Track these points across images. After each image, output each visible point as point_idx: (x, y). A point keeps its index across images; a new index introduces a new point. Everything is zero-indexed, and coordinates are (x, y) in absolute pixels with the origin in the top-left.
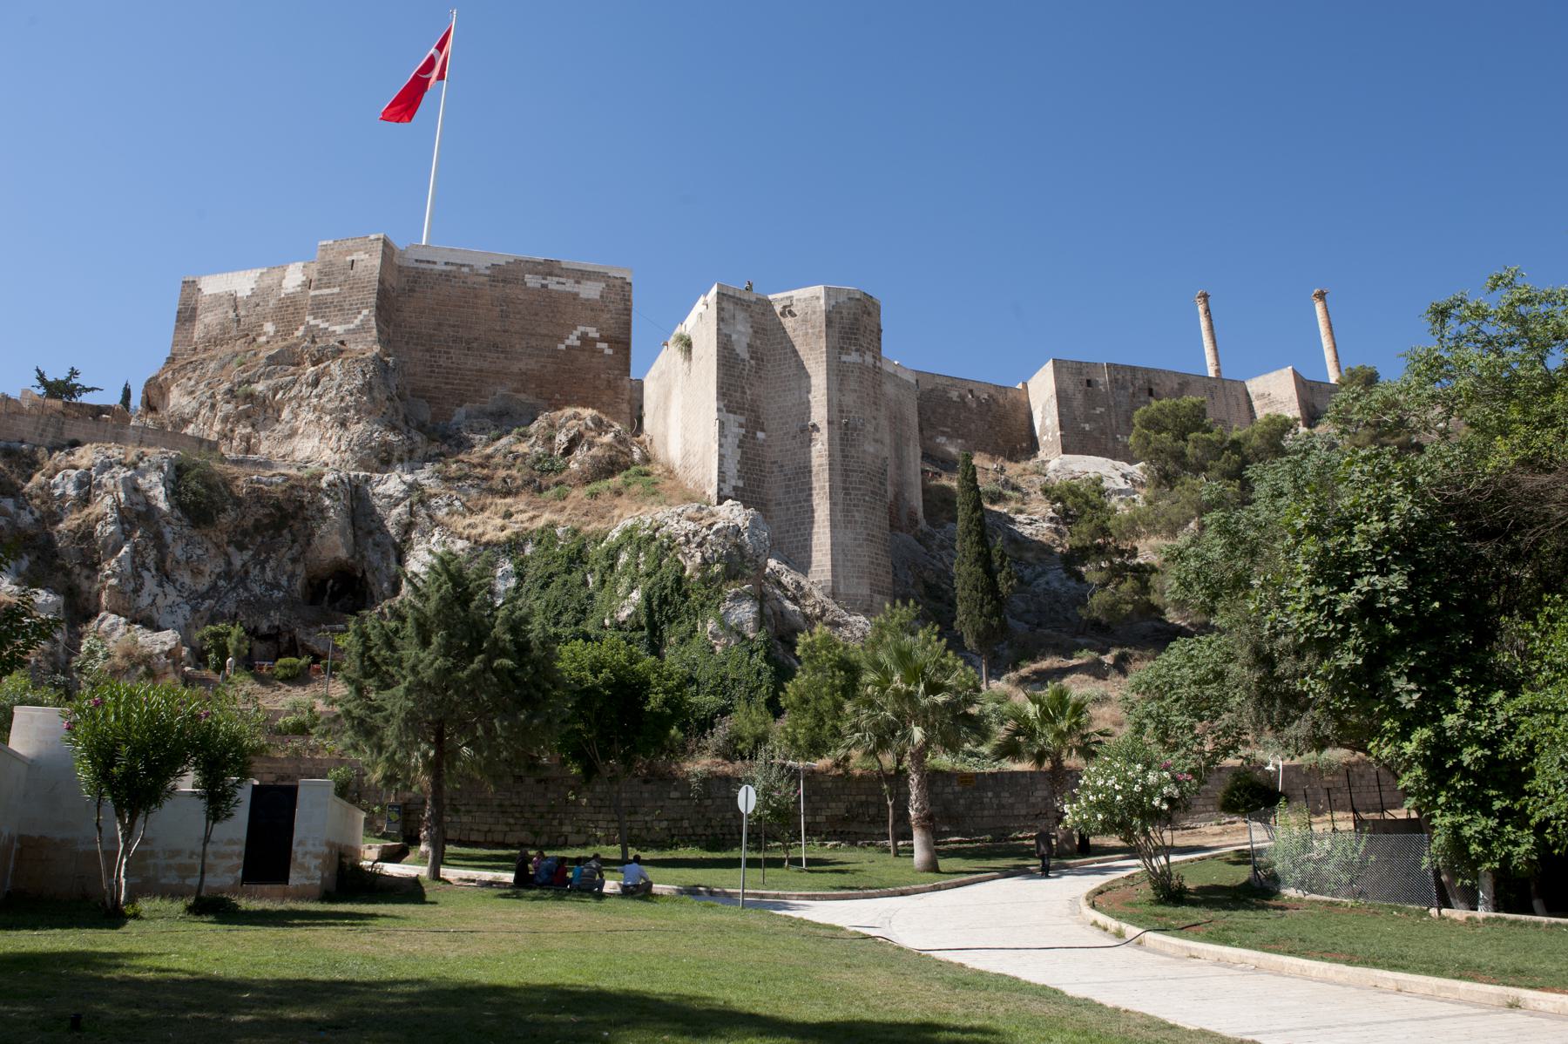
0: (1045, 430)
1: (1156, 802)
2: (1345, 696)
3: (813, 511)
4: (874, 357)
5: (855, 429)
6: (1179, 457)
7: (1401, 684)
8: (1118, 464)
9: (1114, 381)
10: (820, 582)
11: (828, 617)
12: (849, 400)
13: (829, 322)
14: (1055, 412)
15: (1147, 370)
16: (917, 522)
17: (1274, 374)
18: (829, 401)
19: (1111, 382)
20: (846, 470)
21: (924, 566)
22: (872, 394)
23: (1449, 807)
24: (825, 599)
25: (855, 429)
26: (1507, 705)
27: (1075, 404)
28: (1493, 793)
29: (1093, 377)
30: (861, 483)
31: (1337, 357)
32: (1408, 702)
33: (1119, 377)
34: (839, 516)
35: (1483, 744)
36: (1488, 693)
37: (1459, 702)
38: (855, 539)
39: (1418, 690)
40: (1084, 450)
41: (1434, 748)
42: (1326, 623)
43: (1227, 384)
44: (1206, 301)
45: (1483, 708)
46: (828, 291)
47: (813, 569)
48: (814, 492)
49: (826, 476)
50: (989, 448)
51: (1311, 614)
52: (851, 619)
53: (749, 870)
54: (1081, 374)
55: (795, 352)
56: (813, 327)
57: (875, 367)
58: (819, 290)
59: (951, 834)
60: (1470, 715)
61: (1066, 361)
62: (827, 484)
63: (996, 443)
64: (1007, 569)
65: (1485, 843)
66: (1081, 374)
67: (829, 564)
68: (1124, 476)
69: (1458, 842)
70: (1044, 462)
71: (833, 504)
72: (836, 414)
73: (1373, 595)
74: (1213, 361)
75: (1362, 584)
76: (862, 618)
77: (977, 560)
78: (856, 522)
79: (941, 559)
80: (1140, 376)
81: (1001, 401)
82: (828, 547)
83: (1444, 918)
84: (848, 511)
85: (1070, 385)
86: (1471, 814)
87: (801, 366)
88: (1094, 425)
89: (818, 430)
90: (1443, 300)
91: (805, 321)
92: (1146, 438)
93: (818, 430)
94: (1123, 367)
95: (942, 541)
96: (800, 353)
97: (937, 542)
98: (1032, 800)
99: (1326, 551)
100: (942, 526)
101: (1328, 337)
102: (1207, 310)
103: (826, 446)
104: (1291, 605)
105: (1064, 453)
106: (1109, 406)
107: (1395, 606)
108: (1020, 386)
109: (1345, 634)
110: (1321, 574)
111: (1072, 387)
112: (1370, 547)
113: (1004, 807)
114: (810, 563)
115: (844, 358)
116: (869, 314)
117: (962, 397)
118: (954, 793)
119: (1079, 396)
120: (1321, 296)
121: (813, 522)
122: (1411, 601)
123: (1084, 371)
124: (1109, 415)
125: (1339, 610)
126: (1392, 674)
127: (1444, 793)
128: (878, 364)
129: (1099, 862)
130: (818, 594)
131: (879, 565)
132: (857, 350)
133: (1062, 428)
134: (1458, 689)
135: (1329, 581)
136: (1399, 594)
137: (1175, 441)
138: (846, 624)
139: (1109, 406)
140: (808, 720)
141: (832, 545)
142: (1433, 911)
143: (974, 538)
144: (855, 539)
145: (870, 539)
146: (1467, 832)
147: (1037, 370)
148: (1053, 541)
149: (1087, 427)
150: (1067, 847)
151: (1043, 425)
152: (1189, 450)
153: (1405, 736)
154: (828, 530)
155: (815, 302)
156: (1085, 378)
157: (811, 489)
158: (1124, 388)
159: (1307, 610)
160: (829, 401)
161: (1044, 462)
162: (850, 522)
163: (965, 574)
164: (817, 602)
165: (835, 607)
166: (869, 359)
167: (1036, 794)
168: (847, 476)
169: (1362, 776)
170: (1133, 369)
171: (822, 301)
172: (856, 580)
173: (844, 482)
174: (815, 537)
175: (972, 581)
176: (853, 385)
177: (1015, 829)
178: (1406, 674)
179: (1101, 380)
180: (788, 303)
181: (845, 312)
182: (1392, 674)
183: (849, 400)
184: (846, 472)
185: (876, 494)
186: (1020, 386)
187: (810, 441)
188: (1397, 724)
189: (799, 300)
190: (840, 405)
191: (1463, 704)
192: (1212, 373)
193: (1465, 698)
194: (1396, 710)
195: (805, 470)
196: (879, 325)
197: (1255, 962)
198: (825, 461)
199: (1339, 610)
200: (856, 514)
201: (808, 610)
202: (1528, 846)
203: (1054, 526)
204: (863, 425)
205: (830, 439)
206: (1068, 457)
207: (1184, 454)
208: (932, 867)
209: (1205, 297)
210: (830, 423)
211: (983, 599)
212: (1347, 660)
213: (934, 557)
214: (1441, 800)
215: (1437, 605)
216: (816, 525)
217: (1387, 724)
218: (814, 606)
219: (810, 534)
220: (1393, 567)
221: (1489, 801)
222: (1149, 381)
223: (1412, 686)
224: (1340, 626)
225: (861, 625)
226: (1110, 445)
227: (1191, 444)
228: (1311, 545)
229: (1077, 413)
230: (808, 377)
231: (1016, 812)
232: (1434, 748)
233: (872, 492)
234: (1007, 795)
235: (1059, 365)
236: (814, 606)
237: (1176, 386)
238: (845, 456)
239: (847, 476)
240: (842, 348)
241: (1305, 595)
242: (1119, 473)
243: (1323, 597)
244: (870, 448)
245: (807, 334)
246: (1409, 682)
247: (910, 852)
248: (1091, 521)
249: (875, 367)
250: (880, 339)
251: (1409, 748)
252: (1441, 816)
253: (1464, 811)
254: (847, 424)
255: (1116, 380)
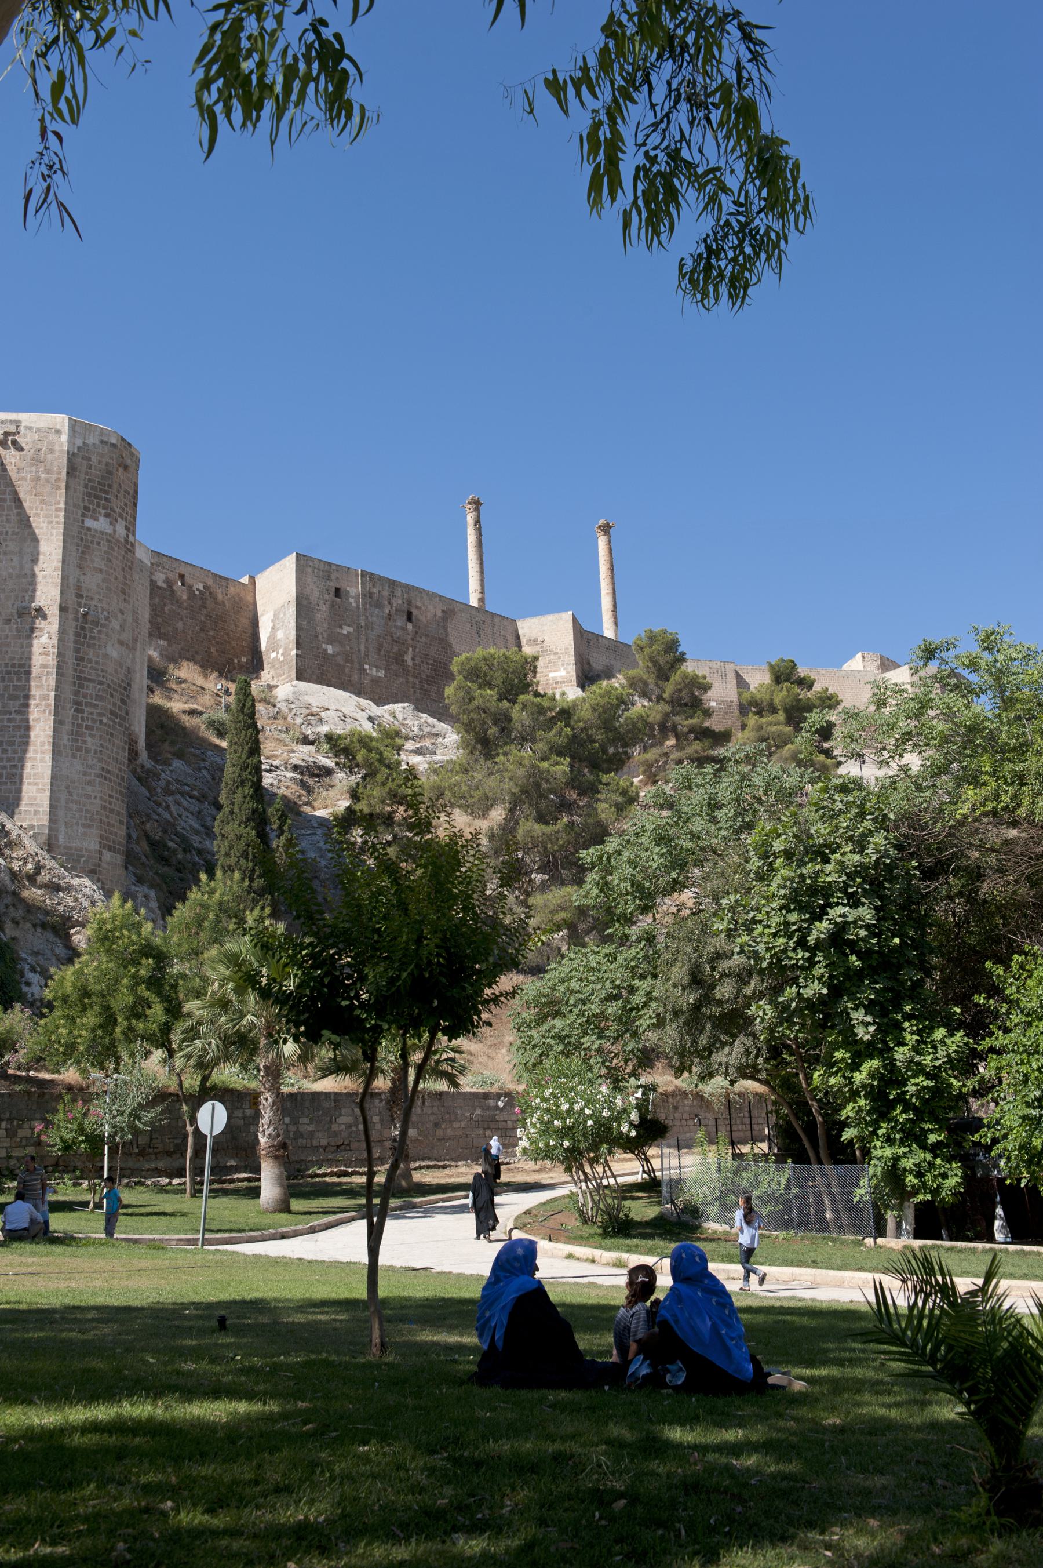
0: (274, 645)
1: (625, 1128)
2: (795, 1024)
3: (28, 728)
4: (127, 529)
5: (96, 623)
6: (503, 720)
7: (858, 1015)
8: (364, 702)
9: (368, 595)
10: (32, 827)
11: (44, 877)
12: (92, 582)
13: (72, 470)
14: (292, 624)
15: (408, 588)
16: (137, 754)
17: (551, 617)
18: (63, 578)
19: (364, 595)
20: (79, 678)
21: (148, 816)
22: (121, 578)
23: (889, 1140)
24: (39, 851)
25: (96, 623)
26: (948, 1041)
27: (318, 617)
28: (928, 1126)
29: (342, 585)
30: (99, 698)
31: (615, 606)
32: (863, 1034)
33: (375, 590)
34: (65, 739)
35: (929, 1076)
36: (932, 1029)
37: (908, 1037)
38: (85, 774)
39: (875, 1023)
40: (323, 680)
41: (882, 1078)
42: (794, 950)
43: (496, 620)
44: (477, 510)
45: (925, 1043)
46: (73, 425)
47: (22, 808)
48: (32, 702)
49: (52, 682)
50: (198, 657)
51: (782, 940)
52: (75, 882)
53: (212, 1202)
54: (329, 578)
55: (18, 501)
56: (48, 471)
57: (127, 541)
58: (61, 421)
59: (237, 1169)
60: (916, 1050)
61: (312, 559)
62: (53, 694)
63: (208, 652)
64: (286, 835)
65: (920, 1175)
66: (329, 578)
67: (46, 803)
68: (370, 719)
69: (893, 1174)
70: (271, 688)
71: (58, 723)
72: (72, 600)
73: (842, 928)
74: (478, 587)
75: (836, 913)
76: (87, 882)
77: (248, 820)
78: (87, 750)
79: (168, 807)
80: (399, 594)
81: (220, 597)
82: (47, 779)
83: (881, 1247)
84: (77, 734)
85: (314, 592)
86: (909, 1146)
87: (25, 523)
88: (338, 649)
89: (44, 617)
90: (936, 638)
91: (36, 460)
92: (468, 691)
93: (44, 617)
94: (381, 578)
95: (168, 783)
96: (26, 505)
97: (162, 783)
98: (335, 1127)
99: (802, 876)
100: (167, 763)
101: (608, 580)
102: (477, 522)
103: (55, 641)
104: (759, 929)
105: (298, 678)
106: (359, 627)
107: (863, 939)
108: (245, 580)
109: (811, 963)
110: (795, 901)
111: (316, 594)
112: (844, 878)
113: (302, 1136)
114: (18, 800)
115: (89, 523)
116: (126, 468)
117: (169, 583)
118: (244, 1118)
119: (324, 608)
120: (606, 529)
121: (27, 744)
122: (877, 935)
123: (333, 577)
124: (358, 638)
125: (811, 939)
126: (850, 1005)
127: (884, 1125)
128: (131, 539)
129: (444, 1200)
130: (30, 845)
131: (112, 811)
132: (107, 515)
133: (298, 645)
134: (906, 1024)
135: (801, 909)
136: (867, 927)
137: (500, 700)
138: (69, 888)
139: (359, 627)
140: (91, 1020)
141: (54, 777)
142: (869, 1241)
143: (248, 790)
144: (85, 774)
145: (105, 775)
146: (908, 1163)
147: (273, 563)
148: (300, 797)
149: (330, 650)
150: (404, 1183)
151: (272, 636)
152: (516, 713)
153: (855, 1067)
154: (48, 757)
155: (53, 437)
156: (333, 585)
157: (27, 697)
158: (379, 605)
159: (775, 935)
160: (64, 578)
161: (271, 688)
162: (79, 749)
163: (232, 836)
164: (29, 855)
165: (52, 863)
166: (121, 530)
167: (340, 1120)
168: (81, 686)
169: (676, 1108)
170: (393, 583)
171: (64, 438)
172: (81, 829)
173: (76, 693)
174: (28, 765)
175: (241, 846)
176: (98, 562)
177: (314, 1164)
178: (864, 1007)
179: (352, 591)
180: (12, 429)
181: (94, 459)
182: (850, 1005)
183: (92, 582)
184: (80, 681)
185: (116, 715)
186: (245, 580)
187: (32, 630)
188: (848, 1055)
189: (30, 428)
190: (79, 588)
191: (911, 1039)
192: (474, 601)
193: (912, 1033)
194: (850, 1040)
195: (23, 670)
196: (136, 485)
197: (811, 1278)
198: (52, 661)
199: (811, 939)
200: (89, 739)
201: (16, 865)
202: (956, 1179)
203: (299, 777)
204: (107, 619)
205: (62, 632)
206: (303, 685)
207: (509, 720)
208: (284, 1207)
209: (477, 504)
210: (63, 609)
211: (253, 870)
212: (813, 989)
213: (159, 805)
214: (881, 1132)
215: (897, 940)
216: (31, 748)
217: (839, 1055)
218: (25, 861)
219: (22, 760)
220: (863, 900)
221: (925, 1133)
222: (409, 603)
223: (869, 1019)
224: (807, 955)
225: (88, 891)
226: (355, 677)
227: (517, 707)
228: (784, 872)
229: (319, 629)
230: (36, 540)
231: (315, 1143)
232: (882, 1078)
233: (112, 712)
234: (306, 1120)
235: (302, 562)
236: (25, 861)
237: (439, 614)
238: (79, 659)
239: (81, 686)
240: (86, 508)
241: (776, 920)
242: (365, 715)
243: (794, 924)
244: (114, 652)
245: (38, 478)
246: (866, 1014)
247: (255, 1193)
248: (384, 784)
249: (127, 541)
250: (135, 505)
251: (859, 1077)
252: (882, 1147)
253: (902, 1143)
254: (86, 614)
255: (371, 595)
